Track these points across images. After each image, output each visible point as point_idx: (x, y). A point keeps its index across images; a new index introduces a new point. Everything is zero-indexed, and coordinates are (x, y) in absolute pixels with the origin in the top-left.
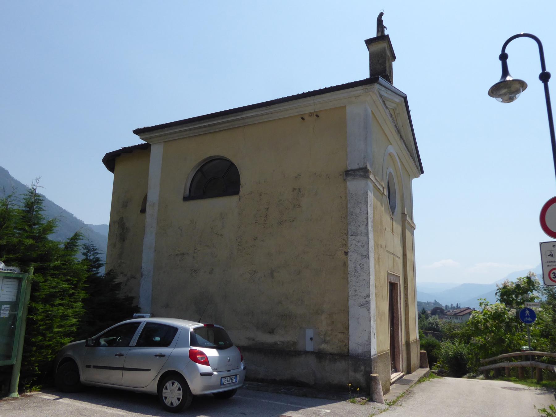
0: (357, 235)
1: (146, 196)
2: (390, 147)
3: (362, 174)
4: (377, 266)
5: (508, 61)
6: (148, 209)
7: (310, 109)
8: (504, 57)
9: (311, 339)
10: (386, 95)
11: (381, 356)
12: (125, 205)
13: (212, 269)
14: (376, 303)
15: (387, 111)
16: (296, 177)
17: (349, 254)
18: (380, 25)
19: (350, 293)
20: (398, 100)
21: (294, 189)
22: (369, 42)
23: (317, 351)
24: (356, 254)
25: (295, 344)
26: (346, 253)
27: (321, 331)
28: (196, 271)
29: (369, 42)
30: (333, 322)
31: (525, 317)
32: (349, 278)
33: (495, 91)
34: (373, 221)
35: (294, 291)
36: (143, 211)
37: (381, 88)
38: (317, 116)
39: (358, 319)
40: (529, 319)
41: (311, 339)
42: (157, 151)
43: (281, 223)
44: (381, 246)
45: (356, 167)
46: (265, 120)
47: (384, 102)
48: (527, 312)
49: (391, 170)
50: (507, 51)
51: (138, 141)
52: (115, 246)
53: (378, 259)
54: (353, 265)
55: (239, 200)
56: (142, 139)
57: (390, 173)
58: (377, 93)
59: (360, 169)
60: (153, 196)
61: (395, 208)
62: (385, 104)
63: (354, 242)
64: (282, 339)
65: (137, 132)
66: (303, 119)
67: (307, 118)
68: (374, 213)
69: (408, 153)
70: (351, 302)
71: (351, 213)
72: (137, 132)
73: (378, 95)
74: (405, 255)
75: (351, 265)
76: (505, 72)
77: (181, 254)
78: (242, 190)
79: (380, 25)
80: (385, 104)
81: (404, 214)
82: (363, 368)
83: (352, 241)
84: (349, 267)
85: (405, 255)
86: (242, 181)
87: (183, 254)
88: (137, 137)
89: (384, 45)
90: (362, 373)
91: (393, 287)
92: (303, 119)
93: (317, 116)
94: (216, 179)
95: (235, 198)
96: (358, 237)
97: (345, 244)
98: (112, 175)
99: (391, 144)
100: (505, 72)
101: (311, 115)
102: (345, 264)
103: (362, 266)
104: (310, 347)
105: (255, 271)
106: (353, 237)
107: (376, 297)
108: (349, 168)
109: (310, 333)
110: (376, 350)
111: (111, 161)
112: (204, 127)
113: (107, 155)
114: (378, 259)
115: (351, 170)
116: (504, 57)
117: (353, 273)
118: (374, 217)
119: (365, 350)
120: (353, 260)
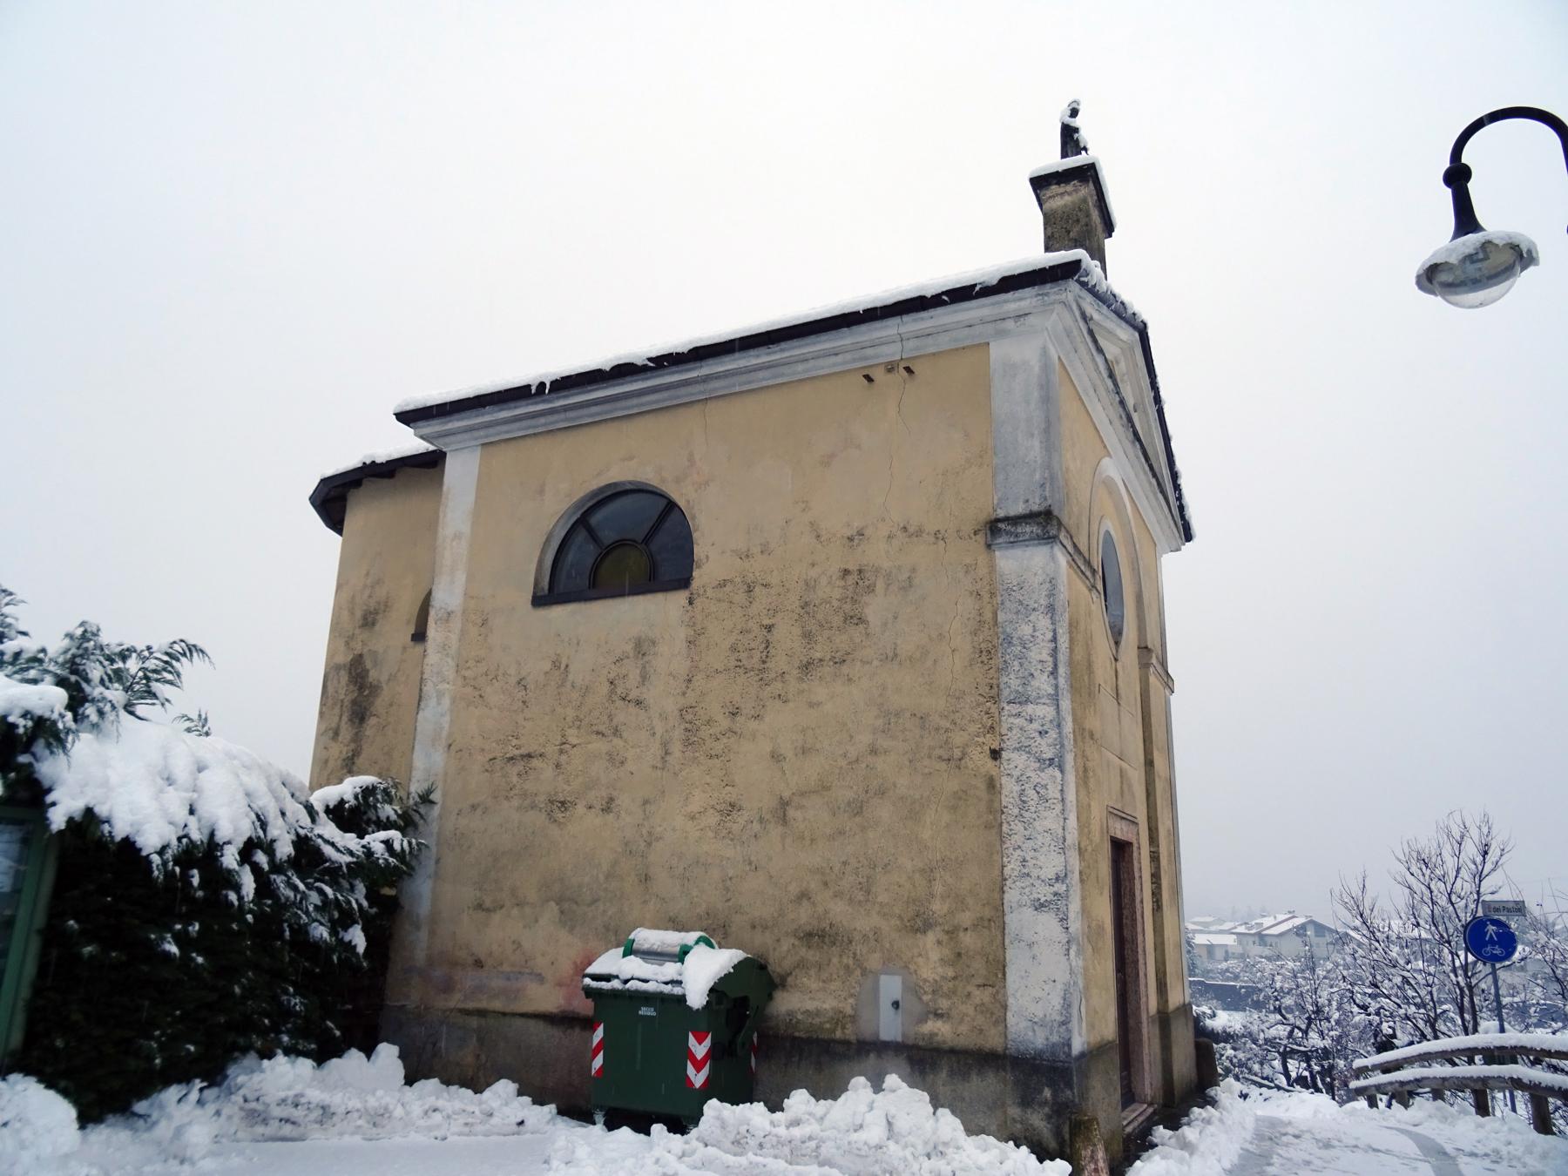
0: (1027, 701)
1: (430, 593)
2: (1106, 461)
3: (1036, 530)
4: (1083, 792)
5: (1472, 186)
6: (432, 631)
7: (892, 352)
8: (1457, 176)
9: (896, 1005)
10: (1096, 316)
11: (1095, 1053)
12: (369, 621)
13: (611, 799)
14: (1083, 899)
15: (1099, 359)
16: (851, 539)
17: (1004, 754)
18: (1070, 139)
19: (1007, 871)
20: (1128, 335)
21: (846, 572)
22: (1040, 183)
23: (910, 1042)
24: (1025, 756)
25: (839, 1019)
26: (995, 754)
27: (925, 981)
28: (563, 803)
29: (1040, 183)
30: (959, 954)
31: (1485, 944)
32: (1005, 828)
33: (1433, 277)
34: (1071, 663)
35: (845, 863)
36: (420, 636)
37: (1084, 293)
38: (908, 370)
39: (1030, 945)
40: (1497, 951)
41: (896, 1005)
42: (461, 470)
43: (807, 667)
44: (1092, 735)
45: (1019, 509)
46: (765, 383)
47: (1091, 332)
48: (1491, 928)
49: (1110, 525)
50: (1466, 158)
51: (408, 442)
52: (336, 733)
53: (1085, 770)
54: (1017, 788)
55: (691, 603)
56: (422, 437)
57: (1108, 533)
58: (1075, 307)
59: (1030, 517)
60: (448, 596)
61: (1120, 633)
62: (1095, 341)
63: (1017, 721)
64: (810, 1005)
65: (407, 417)
66: (869, 379)
67: (878, 375)
68: (1071, 640)
69: (1154, 481)
70: (1011, 896)
71: (1009, 640)
72: (407, 417)
73: (1077, 313)
74: (1149, 763)
75: (1009, 787)
76: (1466, 219)
77: (523, 756)
78: (700, 577)
79: (1070, 139)
80: (1095, 341)
81: (1144, 649)
82: (1047, 1093)
83: (1012, 720)
84: (1004, 792)
85: (1149, 763)
86: (699, 551)
87: (529, 756)
88: (407, 431)
89: (1086, 191)
90: (1047, 1109)
91: (1121, 849)
92: (869, 379)
93: (908, 370)
94: (623, 548)
95: (680, 597)
96: (1030, 708)
97: (992, 727)
98: (335, 539)
99: (1109, 455)
100: (1466, 219)
101: (891, 368)
102: (992, 785)
103: (1042, 792)
104: (890, 1027)
105: (732, 805)
106: (1014, 709)
107: (1082, 881)
108: (1001, 514)
109: (891, 986)
110: (1084, 1039)
111: (334, 499)
112: (596, 402)
113: (324, 482)
114: (1085, 770)
115: (1006, 519)
116: (1457, 176)
117: (1016, 811)
118: (1071, 649)
119: (1055, 1038)
120: (1016, 773)
